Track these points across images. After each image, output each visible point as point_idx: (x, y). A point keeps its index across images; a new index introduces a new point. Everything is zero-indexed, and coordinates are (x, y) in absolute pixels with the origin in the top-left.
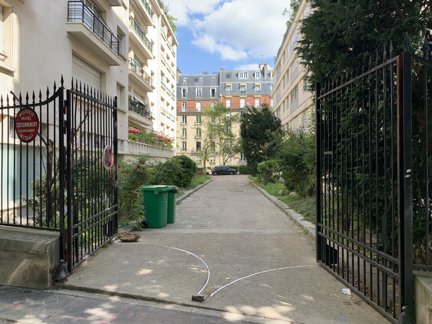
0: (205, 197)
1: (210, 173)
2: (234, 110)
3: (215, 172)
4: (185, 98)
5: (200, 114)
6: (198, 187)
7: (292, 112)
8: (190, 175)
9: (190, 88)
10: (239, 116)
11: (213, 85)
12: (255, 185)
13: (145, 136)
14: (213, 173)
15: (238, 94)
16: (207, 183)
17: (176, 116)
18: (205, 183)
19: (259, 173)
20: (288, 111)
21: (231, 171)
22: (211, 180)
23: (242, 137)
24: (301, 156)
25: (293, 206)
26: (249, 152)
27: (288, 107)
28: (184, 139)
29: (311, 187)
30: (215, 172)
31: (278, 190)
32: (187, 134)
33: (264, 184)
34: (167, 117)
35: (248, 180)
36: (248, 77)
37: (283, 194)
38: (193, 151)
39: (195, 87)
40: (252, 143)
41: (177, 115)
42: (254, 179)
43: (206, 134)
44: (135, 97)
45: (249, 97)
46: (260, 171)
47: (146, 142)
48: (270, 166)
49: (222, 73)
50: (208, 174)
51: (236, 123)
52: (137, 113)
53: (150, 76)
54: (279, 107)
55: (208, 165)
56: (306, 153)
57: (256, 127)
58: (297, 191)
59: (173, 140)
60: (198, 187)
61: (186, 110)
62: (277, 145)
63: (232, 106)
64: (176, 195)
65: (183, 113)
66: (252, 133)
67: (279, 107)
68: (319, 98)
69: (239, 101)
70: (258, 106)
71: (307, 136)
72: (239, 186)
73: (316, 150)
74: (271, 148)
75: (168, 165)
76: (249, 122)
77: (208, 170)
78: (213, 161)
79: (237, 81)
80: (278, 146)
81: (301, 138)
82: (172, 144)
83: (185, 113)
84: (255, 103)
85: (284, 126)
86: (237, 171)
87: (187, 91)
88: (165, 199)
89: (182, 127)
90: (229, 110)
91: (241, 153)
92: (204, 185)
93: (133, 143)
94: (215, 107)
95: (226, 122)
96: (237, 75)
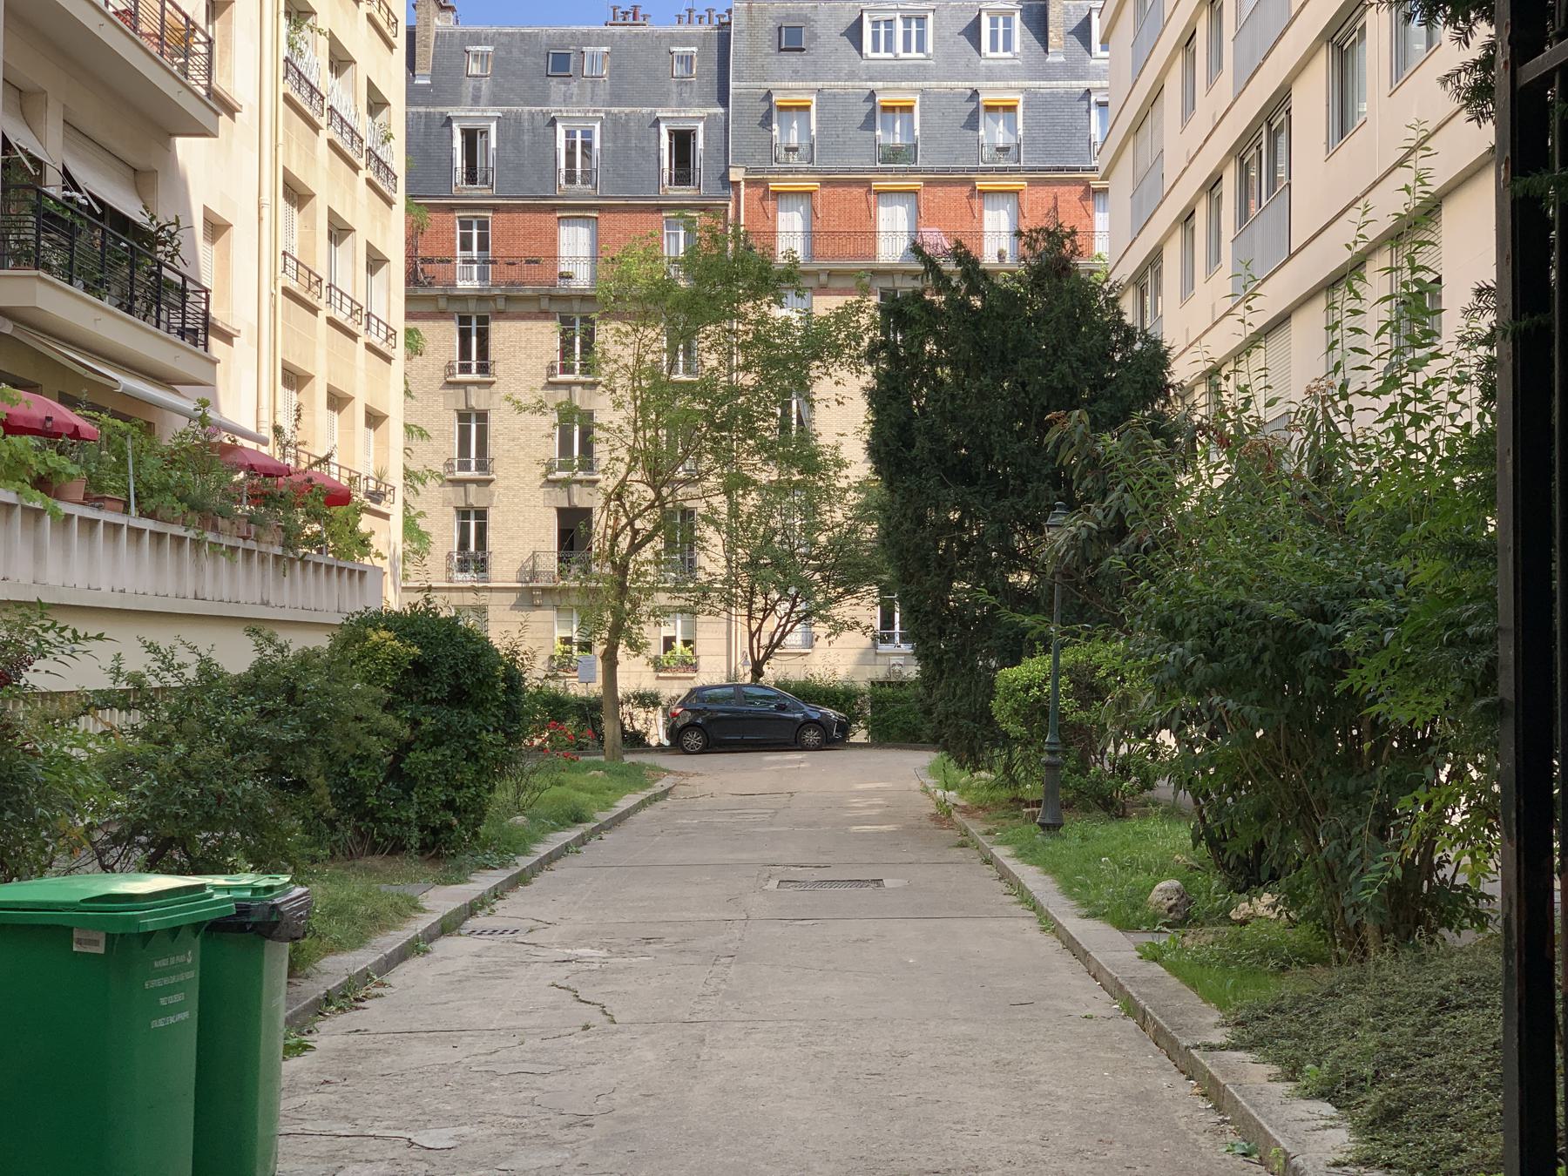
0: (580, 939)
1: (657, 734)
2: (827, 281)
3: (691, 726)
4: (478, 192)
5: (586, 307)
6: (542, 850)
7: (1246, 291)
8: (472, 756)
9: (518, 119)
10: (864, 320)
11: (682, 103)
12: (976, 828)
13: (139, 463)
14: (677, 735)
15: (859, 161)
16: (620, 819)
17: (399, 323)
18: (603, 817)
19: (1006, 740)
20: (1216, 288)
21: (809, 723)
22: (658, 788)
23: (877, 472)
24: (1323, 616)
25: (1262, 1028)
26: (929, 582)
27: (1215, 256)
28: (472, 488)
29: (1407, 866)
30: (686, 727)
31: (1142, 878)
32: (492, 451)
33: (1042, 825)
34: (331, 322)
35: (925, 790)
36: (930, 48)
37: (1183, 917)
38: (534, 575)
39: (553, 110)
40: (954, 516)
41: (409, 316)
42: (968, 787)
43: (622, 453)
44: (73, 171)
45: (940, 191)
46: (1015, 729)
47: (150, 504)
48: (1089, 690)
49: (744, 19)
50: (636, 741)
51: (843, 374)
52: (87, 288)
53: (200, 19)
54: (1154, 260)
55: (633, 674)
56: (1362, 593)
57: (982, 396)
58: (1294, 899)
59: (376, 496)
60: (542, 850)
61: (483, 276)
62: (1141, 533)
63: (819, 249)
64: (278, 956)
65: (463, 298)
66: (957, 446)
67: (1154, 260)
68: (1534, 69)
69: (871, 217)
70: (1001, 255)
71: (1369, 460)
72: (864, 837)
73: (1503, 578)
74: (1094, 553)
75: (270, 693)
76: (934, 361)
77: (640, 713)
78: (678, 645)
79: (852, 76)
80: (1148, 541)
81: (1322, 475)
82: (365, 523)
83: (481, 298)
84: (979, 235)
85: (1185, 391)
86: (854, 718)
87: (493, 144)
88: (177, 998)
89: (457, 399)
90: (790, 279)
91: (884, 590)
92: (597, 831)
93: (38, 513)
94: (689, 262)
95: (771, 362)
96: (854, 33)
